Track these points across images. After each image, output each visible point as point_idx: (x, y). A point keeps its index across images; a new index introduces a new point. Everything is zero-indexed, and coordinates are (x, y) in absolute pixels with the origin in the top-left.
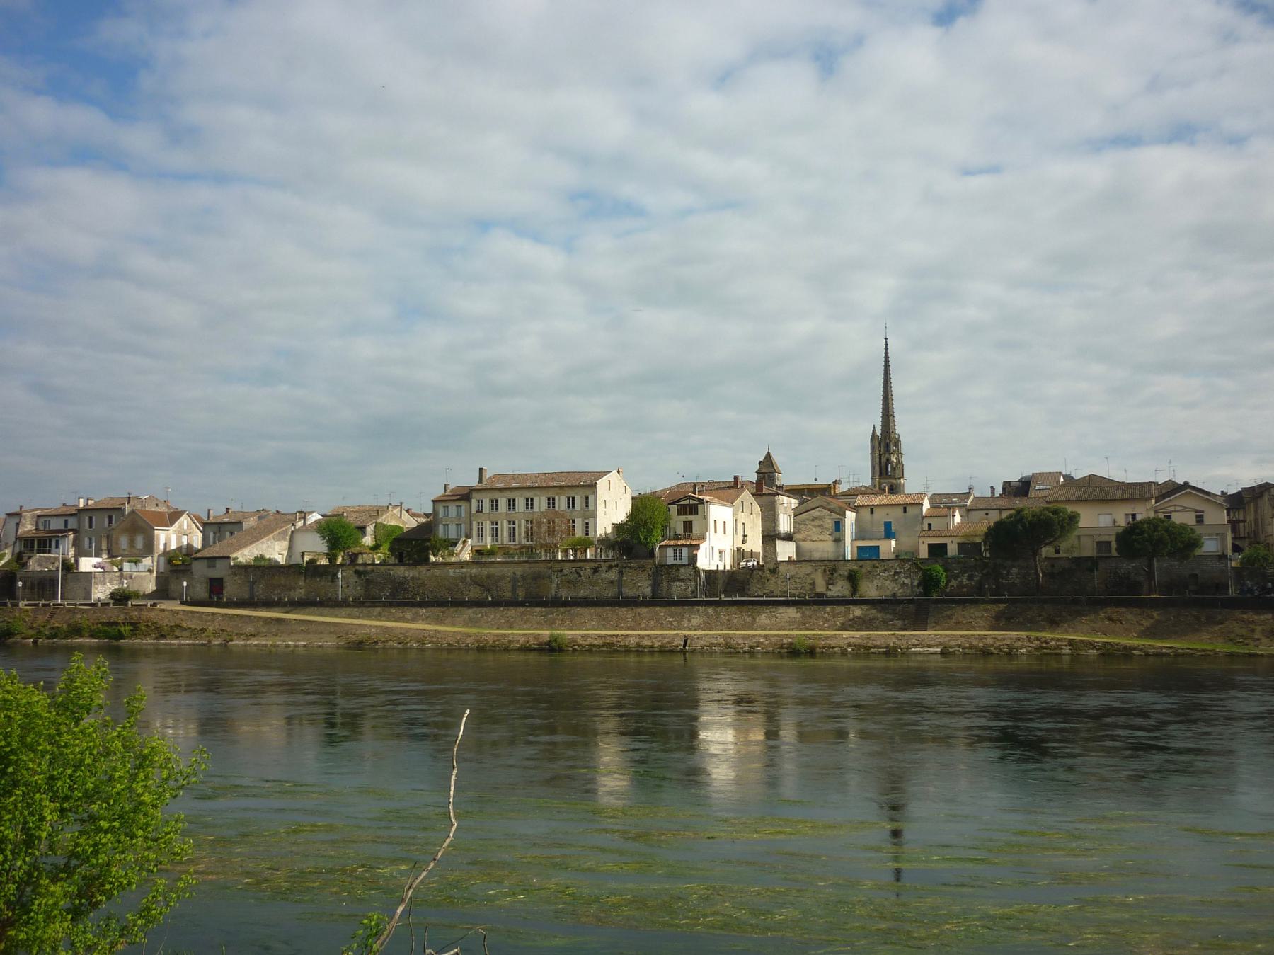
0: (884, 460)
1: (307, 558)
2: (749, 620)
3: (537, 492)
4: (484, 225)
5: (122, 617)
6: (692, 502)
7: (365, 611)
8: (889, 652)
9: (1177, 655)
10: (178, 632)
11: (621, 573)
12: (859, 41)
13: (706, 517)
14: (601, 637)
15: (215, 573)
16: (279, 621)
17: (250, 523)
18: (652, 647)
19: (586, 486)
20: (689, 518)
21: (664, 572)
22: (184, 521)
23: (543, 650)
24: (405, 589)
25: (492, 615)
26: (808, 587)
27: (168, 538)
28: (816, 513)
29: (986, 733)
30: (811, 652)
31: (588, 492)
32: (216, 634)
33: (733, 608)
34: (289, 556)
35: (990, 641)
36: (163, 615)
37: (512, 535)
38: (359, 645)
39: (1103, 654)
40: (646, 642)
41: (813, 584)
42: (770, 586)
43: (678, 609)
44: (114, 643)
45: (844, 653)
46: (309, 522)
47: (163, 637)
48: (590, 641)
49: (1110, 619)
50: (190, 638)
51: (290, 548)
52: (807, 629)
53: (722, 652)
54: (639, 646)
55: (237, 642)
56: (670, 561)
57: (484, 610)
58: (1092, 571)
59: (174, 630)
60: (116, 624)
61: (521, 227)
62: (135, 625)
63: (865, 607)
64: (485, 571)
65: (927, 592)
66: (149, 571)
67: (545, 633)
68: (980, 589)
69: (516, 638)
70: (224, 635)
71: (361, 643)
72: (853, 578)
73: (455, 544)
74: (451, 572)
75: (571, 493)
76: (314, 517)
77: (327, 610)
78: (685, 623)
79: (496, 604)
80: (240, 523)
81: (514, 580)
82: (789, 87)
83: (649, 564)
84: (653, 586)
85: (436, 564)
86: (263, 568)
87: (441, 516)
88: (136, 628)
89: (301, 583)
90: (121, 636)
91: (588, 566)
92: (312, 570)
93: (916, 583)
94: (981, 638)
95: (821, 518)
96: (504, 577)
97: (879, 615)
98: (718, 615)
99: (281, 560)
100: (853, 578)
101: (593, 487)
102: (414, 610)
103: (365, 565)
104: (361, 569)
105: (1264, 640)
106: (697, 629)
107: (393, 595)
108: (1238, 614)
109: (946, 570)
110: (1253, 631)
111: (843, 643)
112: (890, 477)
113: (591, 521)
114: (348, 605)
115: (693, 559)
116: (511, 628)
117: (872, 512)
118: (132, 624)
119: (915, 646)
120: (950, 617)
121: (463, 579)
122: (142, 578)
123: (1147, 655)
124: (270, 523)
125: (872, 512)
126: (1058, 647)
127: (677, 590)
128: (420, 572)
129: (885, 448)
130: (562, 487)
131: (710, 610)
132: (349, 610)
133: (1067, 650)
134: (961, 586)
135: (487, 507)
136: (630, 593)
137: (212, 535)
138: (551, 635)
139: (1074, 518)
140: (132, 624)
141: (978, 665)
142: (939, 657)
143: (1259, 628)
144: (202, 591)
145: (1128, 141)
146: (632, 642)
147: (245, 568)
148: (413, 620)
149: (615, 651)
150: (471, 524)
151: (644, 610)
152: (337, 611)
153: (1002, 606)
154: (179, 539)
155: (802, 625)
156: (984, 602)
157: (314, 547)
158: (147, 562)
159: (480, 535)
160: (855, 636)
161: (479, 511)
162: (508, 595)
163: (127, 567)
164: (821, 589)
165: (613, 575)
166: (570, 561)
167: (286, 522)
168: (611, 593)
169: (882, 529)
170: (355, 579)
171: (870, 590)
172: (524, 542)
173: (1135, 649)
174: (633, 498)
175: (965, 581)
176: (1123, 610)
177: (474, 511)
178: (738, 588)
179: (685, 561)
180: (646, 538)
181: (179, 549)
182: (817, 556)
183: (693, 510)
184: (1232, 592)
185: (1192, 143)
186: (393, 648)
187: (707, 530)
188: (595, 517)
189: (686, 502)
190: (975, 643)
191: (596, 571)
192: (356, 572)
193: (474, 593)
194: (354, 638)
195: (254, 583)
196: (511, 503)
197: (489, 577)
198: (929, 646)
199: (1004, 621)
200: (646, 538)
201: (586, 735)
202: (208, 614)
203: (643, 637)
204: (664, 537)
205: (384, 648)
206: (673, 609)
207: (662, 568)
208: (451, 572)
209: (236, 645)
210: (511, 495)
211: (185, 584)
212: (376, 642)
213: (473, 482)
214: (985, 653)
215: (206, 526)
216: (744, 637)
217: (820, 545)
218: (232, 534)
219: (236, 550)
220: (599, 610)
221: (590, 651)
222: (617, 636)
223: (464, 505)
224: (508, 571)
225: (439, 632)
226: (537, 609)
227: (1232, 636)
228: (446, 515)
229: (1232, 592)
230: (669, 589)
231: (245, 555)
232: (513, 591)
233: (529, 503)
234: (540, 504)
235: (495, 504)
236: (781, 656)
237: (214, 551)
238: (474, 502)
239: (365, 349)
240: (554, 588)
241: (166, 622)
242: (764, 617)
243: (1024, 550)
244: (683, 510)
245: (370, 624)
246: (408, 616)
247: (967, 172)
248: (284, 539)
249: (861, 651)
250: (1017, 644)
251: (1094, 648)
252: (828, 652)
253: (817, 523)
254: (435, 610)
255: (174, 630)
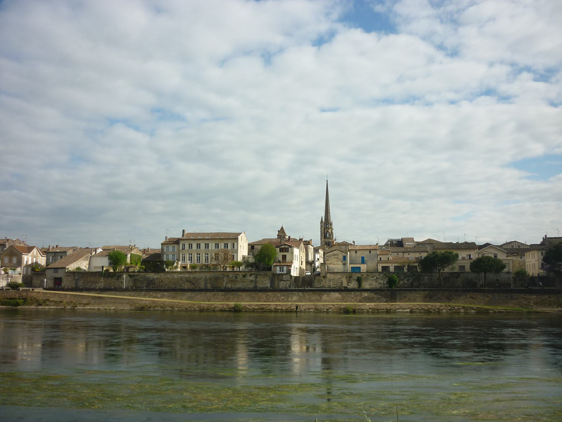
0: (326, 231)
1: (105, 269)
2: (318, 298)
3: (211, 241)
4: (113, 121)
5: (17, 295)
6: (286, 247)
7: (137, 293)
8: (388, 311)
9: (507, 312)
10: (48, 303)
11: (256, 277)
12: (281, 50)
13: (292, 253)
14: (258, 305)
15: (58, 275)
16: (99, 297)
17: (70, 252)
18: (282, 309)
19: (234, 238)
20: (285, 254)
21: (276, 277)
22: (35, 251)
23: (231, 311)
24: (153, 284)
25: (200, 295)
26: (339, 284)
27: (27, 259)
28: (335, 252)
29: (546, 343)
30: (354, 312)
31: (234, 241)
32: (68, 303)
33: (311, 293)
34: (89, 268)
35: (430, 307)
36: (39, 294)
37: (199, 259)
38: (142, 308)
39: (477, 312)
40: (279, 308)
41: (342, 283)
42: (323, 283)
43: (286, 293)
44: (14, 308)
45: (368, 312)
46: (98, 252)
47: (40, 305)
48: (252, 307)
49: (472, 298)
50: (54, 305)
51: (89, 264)
52: (345, 302)
53: (314, 312)
54: (276, 309)
55: (79, 307)
56: (278, 272)
57: (195, 293)
58: (457, 278)
59: (45, 302)
60: (15, 299)
61: (129, 123)
62: (25, 300)
63: (368, 293)
64: (192, 276)
65: (390, 286)
66: (20, 274)
67: (232, 304)
68: (412, 285)
69: (218, 306)
70: (72, 304)
71: (142, 308)
72: (359, 280)
73: (173, 264)
74: (176, 276)
75: (226, 242)
76: (99, 250)
77: (118, 293)
78: (290, 299)
79: (201, 290)
80: (65, 252)
81: (206, 280)
82: (251, 67)
83: (269, 273)
84: (271, 283)
85: (168, 272)
86: (79, 273)
87: (165, 250)
88: (25, 301)
89: (102, 280)
90: (18, 304)
91: (241, 274)
92: (106, 274)
93: (385, 282)
94: (426, 306)
95: (337, 255)
96: (201, 278)
97: (375, 296)
98: (304, 296)
99: (86, 269)
100: (359, 280)
101: (237, 239)
102: (161, 293)
103: (134, 272)
104: (132, 274)
105: (534, 306)
106: (293, 301)
107: (147, 286)
108: (522, 295)
109: (398, 277)
110: (529, 302)
111: (367, 308)
112: (328, 238)
113: (235, 254)
114: (129, 291)
115: (289, 271)
116: (209, 301)
117: (356, 252)
118: (23, 299)
119: (398, 309)
120: (406, 297)
121: (181, 279)
122: (16, 277)
123: (495, 312)
124: (80, 253)
125: (356, 252)
126: (458, 309)
127: (282, 285)
128: (161, 276)
129: (326, 225)
130: (222, 239)
131: (301, 294)
132: (129, 293)
133: (462, 311)
134: (404, 284)
135: (187, 247)
136: (261, 286)
137: (51, 257)
138: (235, 304)
139: (457, 256)
140: (23, 299)
141: (425, 316)
142: (409, 314)
143: (532, 301)
144: (51, 285)
145: (388, 101)
146: (272, 308)
147: (73, 273)
148: (162, 297)
149: (265, 311)
150: (179, 255)
151: (270, 293)
152: (123, 293)
153: (427, 292)
154: (32, 259)
155: (342, 300)
156: (419, 290)
157: (103, 263)
158: (19, 270)
159: (184, 259)
160: (372, 305)
161: (184, 249)
162: (203, 286)
163: (10, 272)
164: (345, 284)
165: (252, 278)
166: (234, 272)
167: (87, 252)
168: (251, 286)
169: (361, 260)
170: (129, 278)
171: (366, 285)
172: (204, 263)
173: (490, 310)
174: (249, 245)
175: (406, 282)
176: (477, 294)
177: (181, 248)
178: (308, 284)
179: (285, 272)
180: (268, 262)
181: (32, 264)
182: (336, 271)
183: (286, 250)
184: (512, 287)
185: (413, 104)
186: (158, 310)
187: (293, 259)
188: (237, 252)
189: (284, 247)
190: (424, 307)
191: (244, 276)
192: (130, 275)
193: (186, 286)
194: (138, 306)
195: (78, 280)
196: (199, 246)
197: (194, 278)
198: (404, 309)
199: (429, 298)
200: (268, 262)
201: (233, 351)
202: (63, 294)
203: (277, 305)
204: (275, 262)
205: (154, 310)
206: (283, 293)
207: (274, 275)
208: (176, 276)
209: (79, 309)
210: (198, 242)
211: (45, 280)
212: (150, 308)
213: (180, 236)
214: (428, 312)
215: (46, 252)
216: (323, 305)
217: (337, 266)
218: (61, 257)
219: (68, 265)
220: (249, 293)
221: (253, 311)
222: (265, 305)
223: (176, 246)
224: (203, 275)
225: (180, 303)
226: (221, 293)
227: (522, 304)
228: (168, 250)
229: (512, 287)
230: (278, 284)
231: (72, 267)
232: (206, 283)
233: (207, 246)
234: (212, 246)
235: (191, 246)
236: (340, 313)
237: (56, 265)
238: (181, 245)
239: (56, 175)
240: (225, 283)
241: (41, 298)
242: (325, 297)
243: (430, 271)
244: (282, 250)
245: (145, 299)
246: (159, 295)
247: (323, 110)
248: (87, 260)
249: (375, 311)
250: (442, 308)
251: (473, 309)
252: (361, 311)
253: (335, 257)
254: (172, 293)
255: (45, 302)
